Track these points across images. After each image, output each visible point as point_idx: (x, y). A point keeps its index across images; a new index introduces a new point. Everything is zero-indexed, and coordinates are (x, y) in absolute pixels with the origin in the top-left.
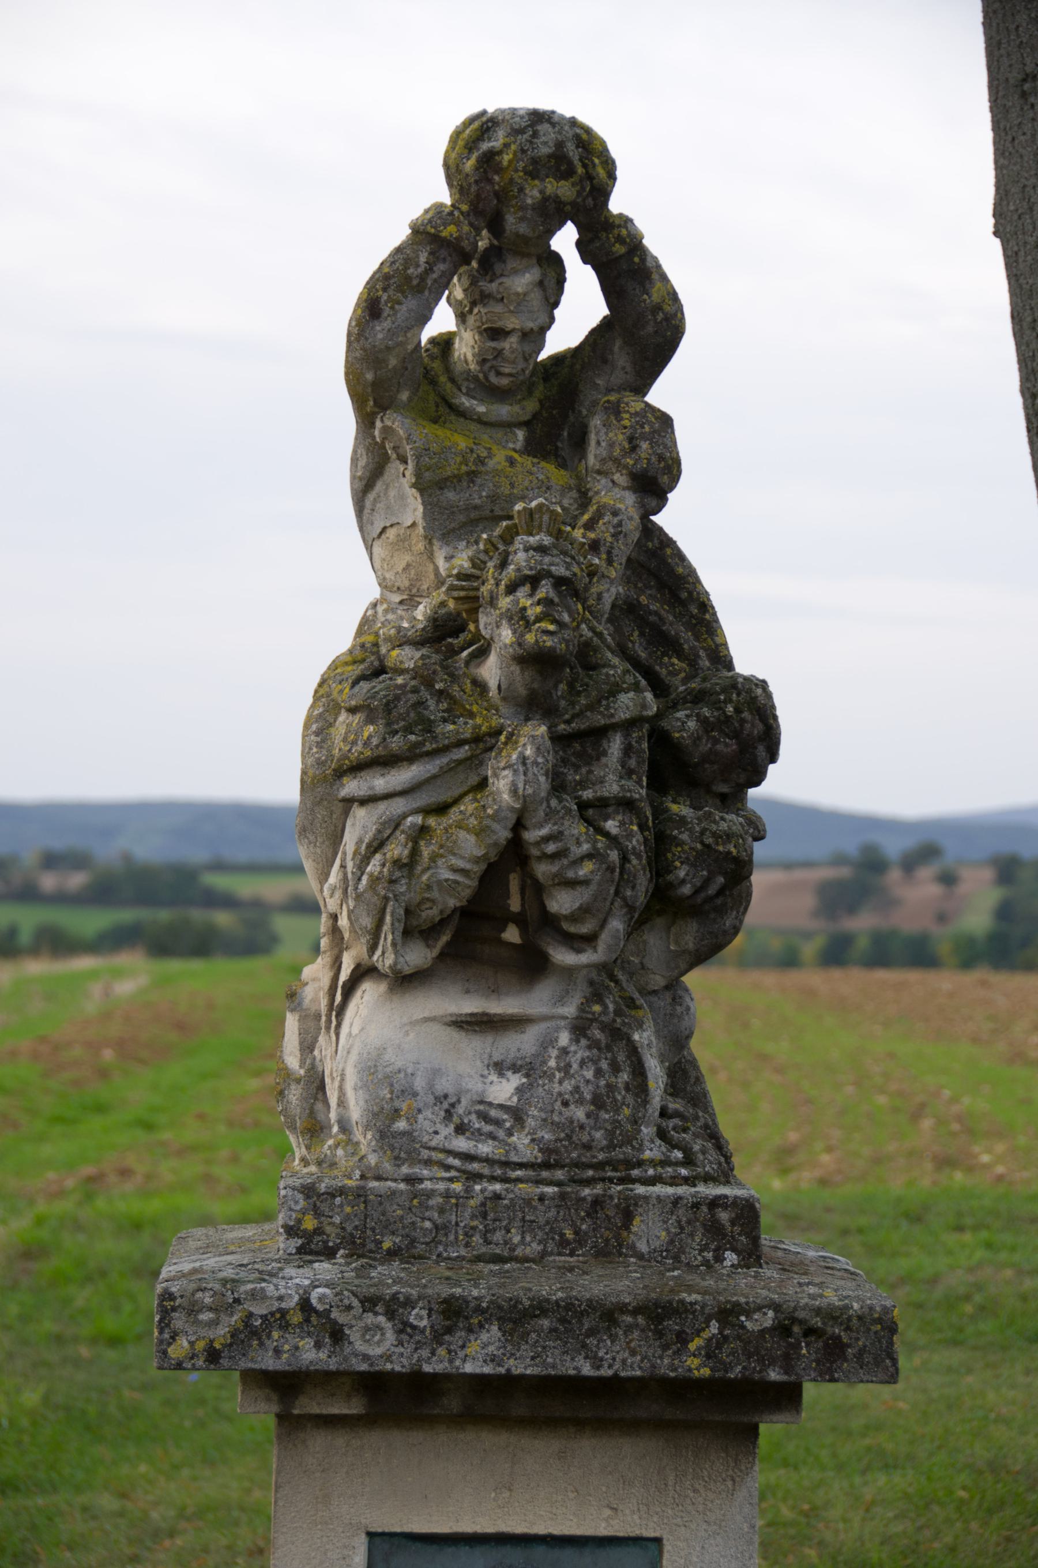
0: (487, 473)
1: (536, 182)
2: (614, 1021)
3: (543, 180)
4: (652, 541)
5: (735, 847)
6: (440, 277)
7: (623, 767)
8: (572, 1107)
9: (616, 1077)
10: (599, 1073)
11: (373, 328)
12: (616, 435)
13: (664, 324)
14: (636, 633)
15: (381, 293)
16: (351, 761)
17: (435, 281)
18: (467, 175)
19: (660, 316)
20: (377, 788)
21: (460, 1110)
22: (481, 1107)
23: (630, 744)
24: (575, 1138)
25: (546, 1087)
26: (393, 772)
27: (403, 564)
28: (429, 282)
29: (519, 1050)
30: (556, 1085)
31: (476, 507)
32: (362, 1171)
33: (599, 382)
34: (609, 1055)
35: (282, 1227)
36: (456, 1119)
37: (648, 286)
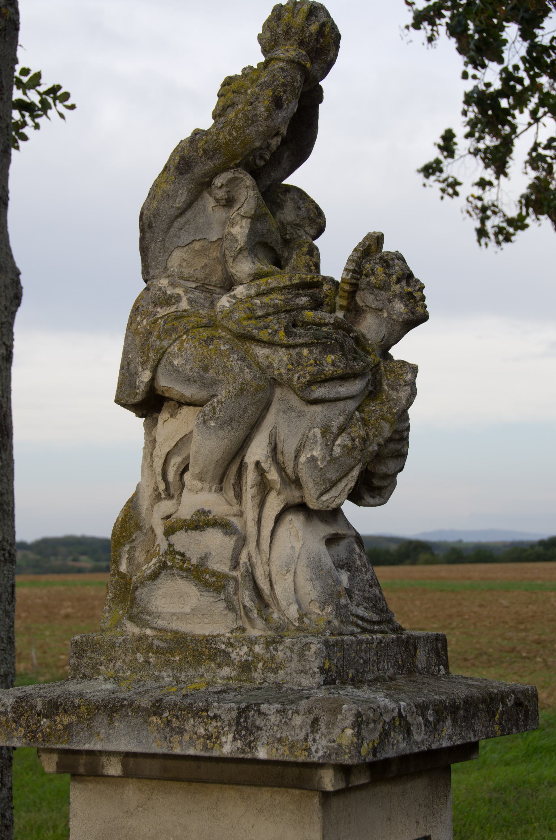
8: (374, 588)
11: (277, 114)
12: (309, 205)
15: (282, 94)
16: (326, 376)
18: (312, 34)
20: (342, 393)
24: (378, 606)
25: (360, 577)
26: (347, 384)
27: (203, 264)
29: (338, 555)
30: (365, 575)
32: (331, 631)
33: (272, 174)
35: (318, 668)
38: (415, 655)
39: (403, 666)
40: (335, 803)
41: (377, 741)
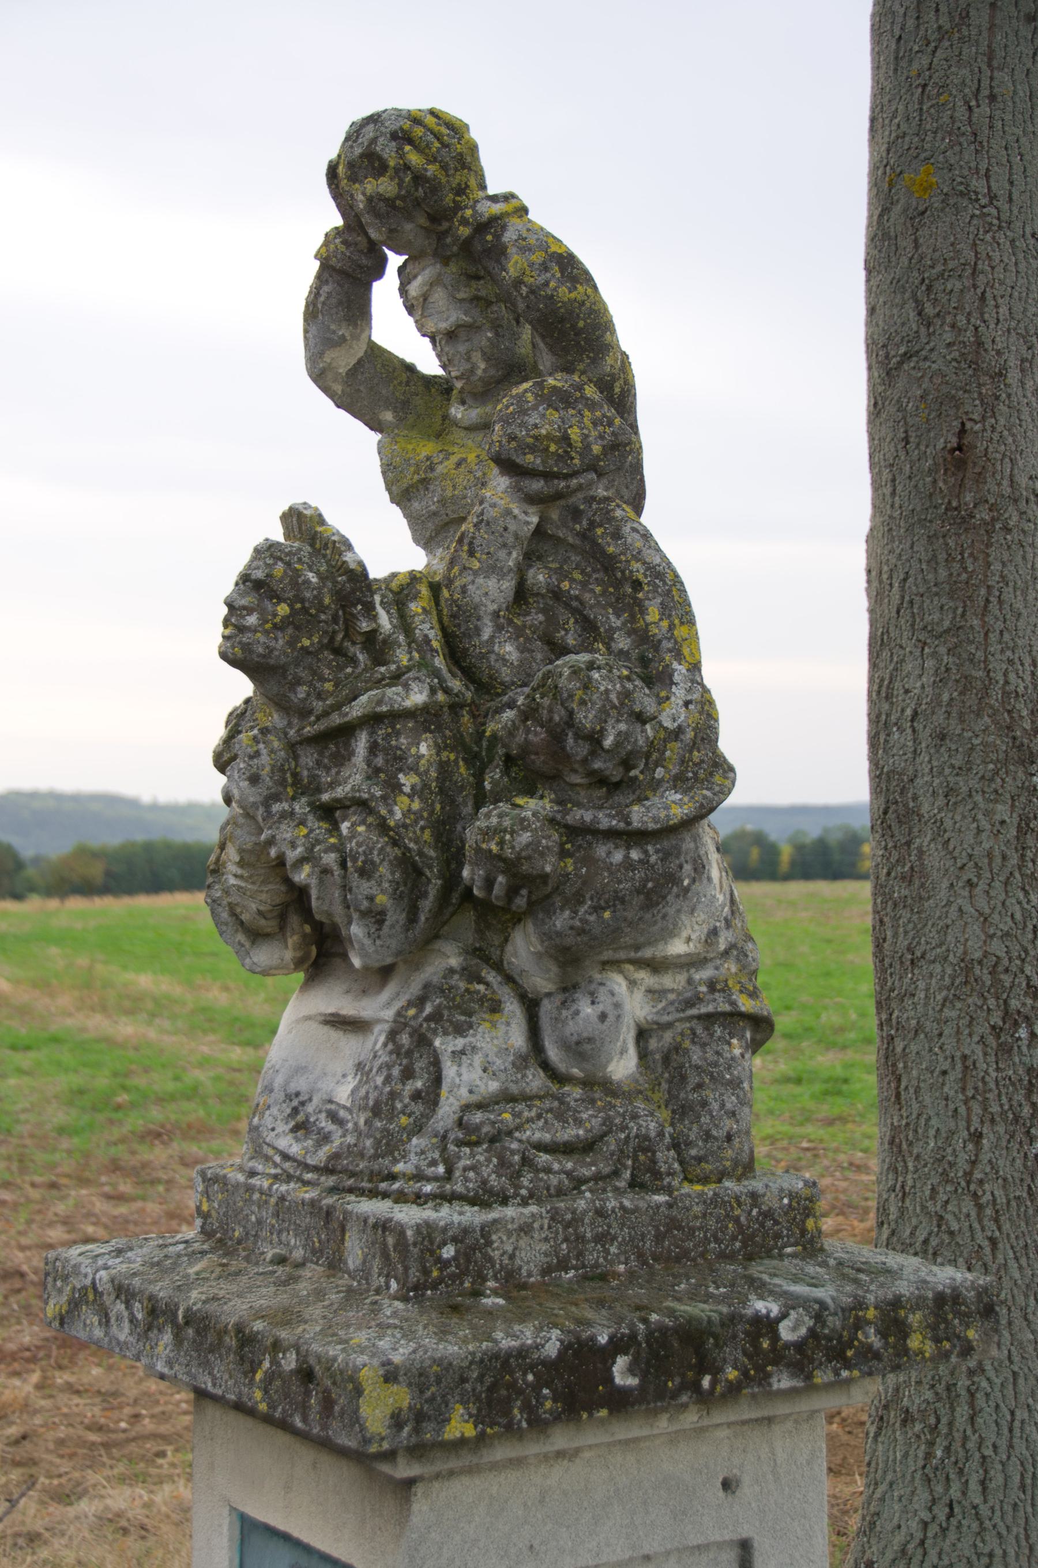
0: (436, 479)
1: (357, 185)
2: (421, 1025)
3: (361, 182)
4: (580, 523)
5: (497, 844)
6: (328, 298)
7: (369, 766)
9: (404, 1084)
10: (388, 1079)
13: (532, 297)
14: (572, 621)
17: (324, 303)
19: (524, 290)
21: (310, 1108)
22: (329, 1106)
23: (375, 742)
28: (320, 306)
31: (435, 514)
34: (405, 1061)
36: (300, 1117)
37: (504, 262)
38: (343, 1240)
39: (321, 1251)
40: (212, 1411)
41: (65, 1308)
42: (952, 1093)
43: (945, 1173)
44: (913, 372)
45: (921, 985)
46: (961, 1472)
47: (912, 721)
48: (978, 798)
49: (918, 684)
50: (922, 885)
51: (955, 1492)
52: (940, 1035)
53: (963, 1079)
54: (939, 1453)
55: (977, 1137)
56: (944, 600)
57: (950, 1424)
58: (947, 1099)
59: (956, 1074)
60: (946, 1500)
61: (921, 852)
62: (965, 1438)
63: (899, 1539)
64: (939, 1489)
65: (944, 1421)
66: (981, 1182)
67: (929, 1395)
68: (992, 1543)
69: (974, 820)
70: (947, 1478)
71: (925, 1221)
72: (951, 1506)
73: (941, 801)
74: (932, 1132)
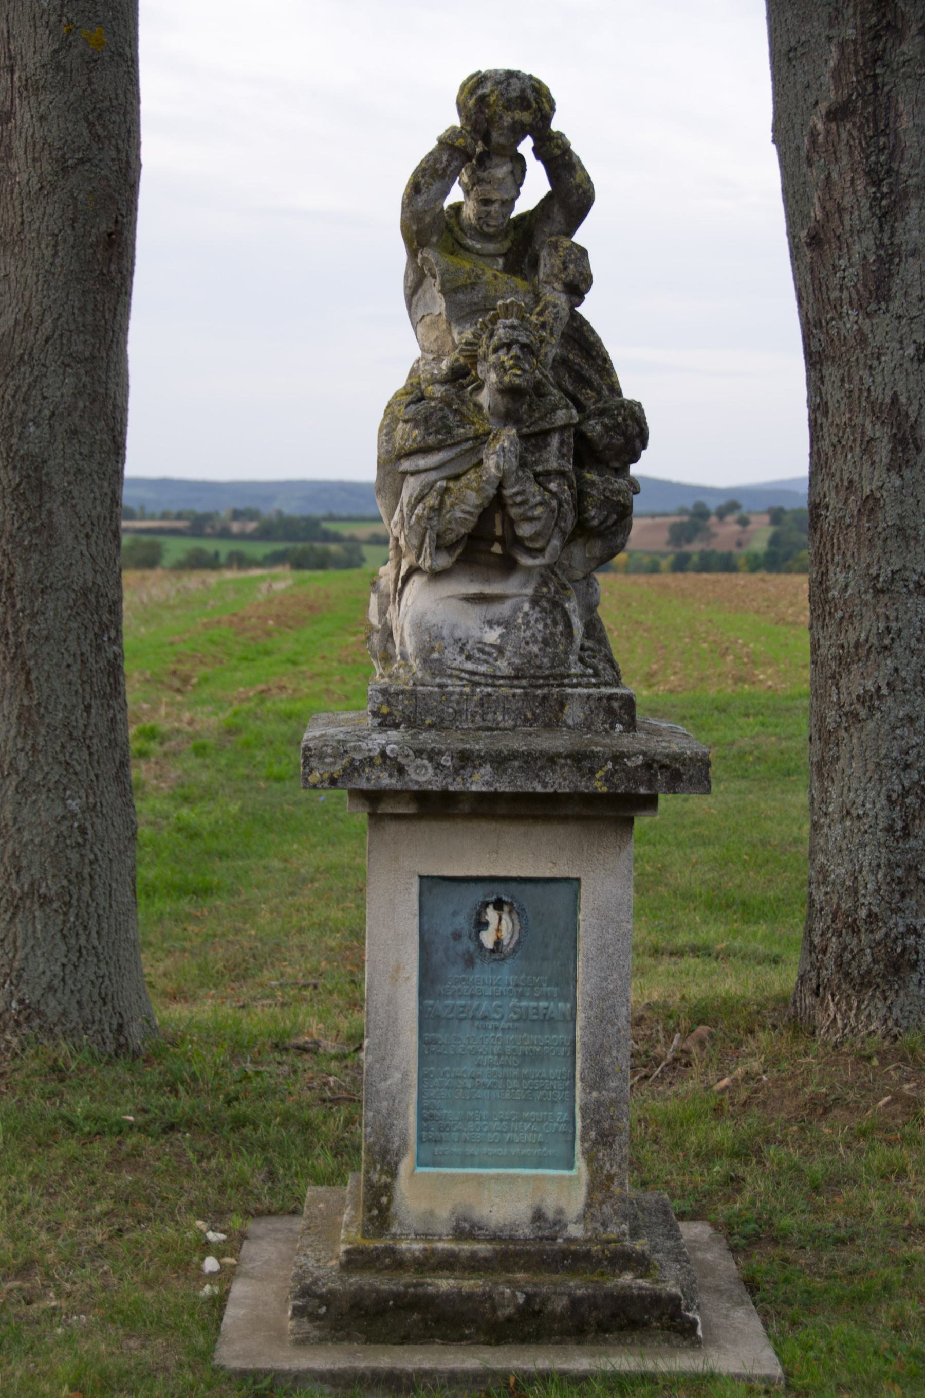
10: (546, 626)
19: (581, 191)
21: (468, 647)
42: (74, 679)
43: (71, 734)
44: (86, 174)
45: (51, 605)
46: (85, 928)
47: (50, 419)
48: (95, 477)
49: (58, 394)
50: (51, 536)
51: (83, 941)
52: (65, 641)
53: (81, 671)
54: (72, 919)
55: (88, 708)
56: (88, 337)
57: (78, 900)
58: (70, 684)
59: (77, 667)
60: (77, 947)
61: (50, 513)
62: (88, 905)
63: (45, 980)
64: (73, 941)
65: (75, 897)
66: (91, 738)
67: (65, 882)
68: (104, 970)
69: (92, 491)
70: (77, 934)
71: (56, 767)
72: (80, 951)
73: (71, 478)
74: (60, 707)
